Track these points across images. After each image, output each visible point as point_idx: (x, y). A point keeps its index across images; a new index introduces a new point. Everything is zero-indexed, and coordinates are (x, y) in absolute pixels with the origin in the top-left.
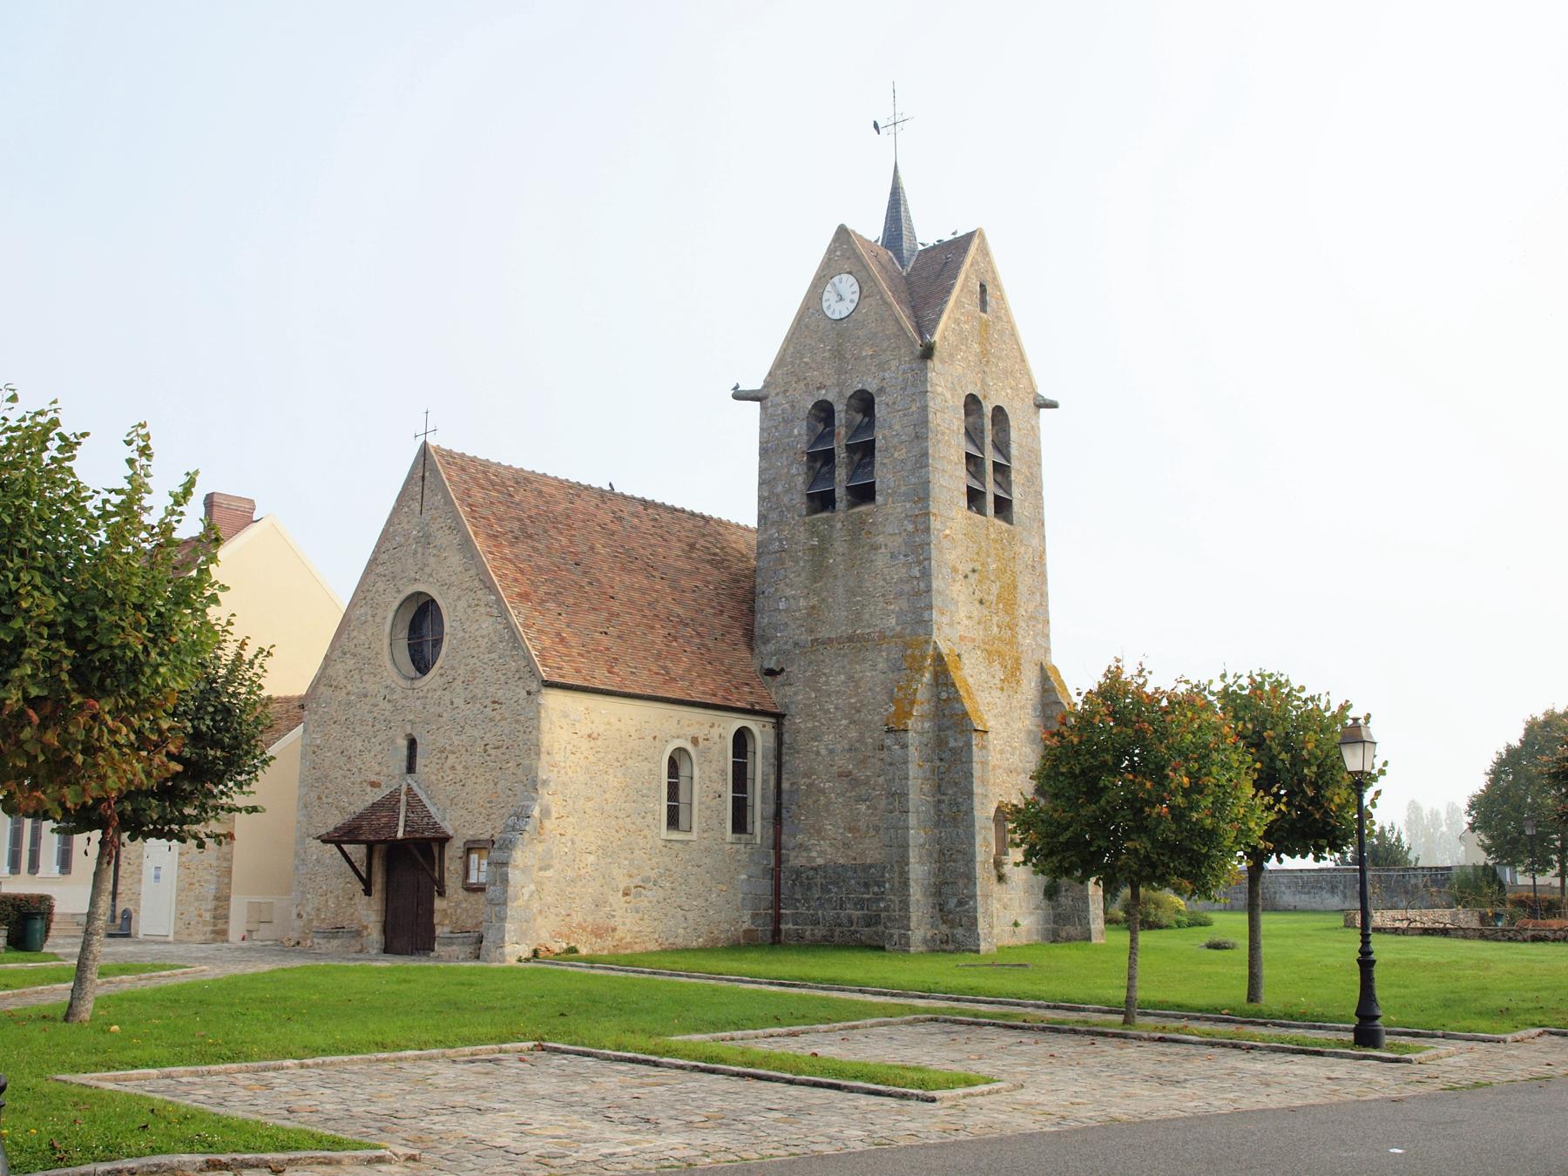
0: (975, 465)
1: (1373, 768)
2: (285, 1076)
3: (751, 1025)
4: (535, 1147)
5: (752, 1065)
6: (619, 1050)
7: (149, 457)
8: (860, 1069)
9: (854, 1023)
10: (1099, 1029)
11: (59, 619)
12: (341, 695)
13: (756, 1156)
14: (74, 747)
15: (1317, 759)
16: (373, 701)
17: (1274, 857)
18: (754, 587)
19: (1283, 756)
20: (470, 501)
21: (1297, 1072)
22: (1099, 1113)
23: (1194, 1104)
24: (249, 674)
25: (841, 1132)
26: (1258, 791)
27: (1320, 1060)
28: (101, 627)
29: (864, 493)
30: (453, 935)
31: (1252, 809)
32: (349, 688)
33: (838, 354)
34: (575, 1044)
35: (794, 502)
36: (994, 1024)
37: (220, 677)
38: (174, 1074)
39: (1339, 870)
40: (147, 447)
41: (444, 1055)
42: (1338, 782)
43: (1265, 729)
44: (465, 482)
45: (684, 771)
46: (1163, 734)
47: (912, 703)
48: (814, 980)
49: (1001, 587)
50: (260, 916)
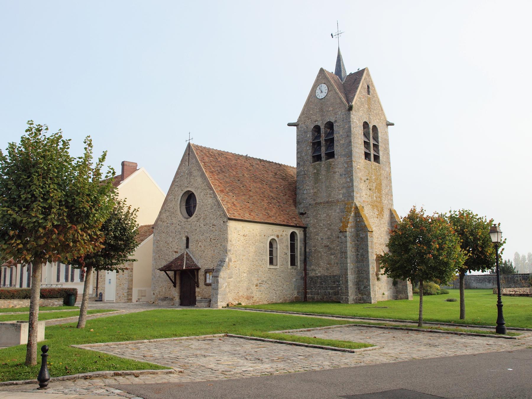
0: (367, 144)
1: (501, 241)
2: (144, 345)
3: (295, 328)
4: (221, 368)
5: (294, 341)
6: (251, 336)
7: (91, 147)
8: (329, 342)
9: (329, 327)
10: (410, 328)
11: (63, 200)
12: (165, 224)
13: (293, 371)
14: (70, 240)
15: (482, 238)
16: (175, 225)
17: (468, 271)
18: (296, 186)
19: (471, 237)
20: (204, 161)
21: (476, 342)
22: (409, 356)
23: (441, 353)
24: (132, 217)
25: (322, 363)
26: (462, 249)
27: (485, 338)
28: (76, 201)
29: (331, 155)
30: (202, 300)
31: (460, 255)
32: (167, 222)
33: (321, 110)
34: (238, 334)
35: (308, 159)
36: (375, 327)
37: (122, 218)
38: (109, 345)
39: (491, 275)
40: (90, 144)
41: (195, 338)
42: (489, 246)
43: (465, 229)
44: (202, 155)
45: (274, 246)
46: (430, 231)
47: (348, 223)
48: (317, 313)
49: (376, 184)
50: (142, 294)
